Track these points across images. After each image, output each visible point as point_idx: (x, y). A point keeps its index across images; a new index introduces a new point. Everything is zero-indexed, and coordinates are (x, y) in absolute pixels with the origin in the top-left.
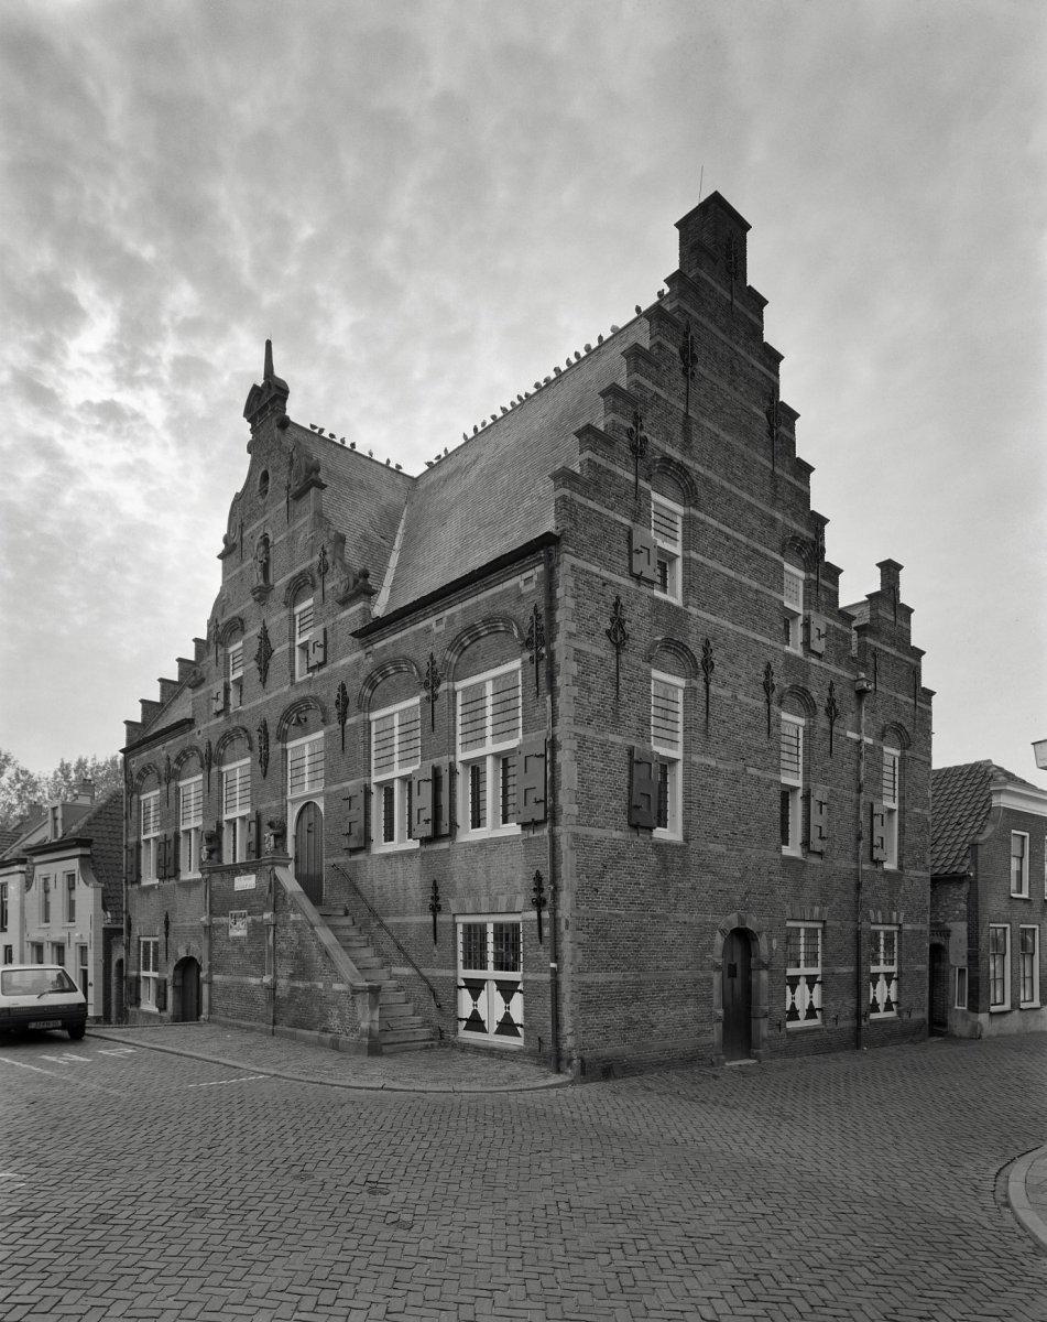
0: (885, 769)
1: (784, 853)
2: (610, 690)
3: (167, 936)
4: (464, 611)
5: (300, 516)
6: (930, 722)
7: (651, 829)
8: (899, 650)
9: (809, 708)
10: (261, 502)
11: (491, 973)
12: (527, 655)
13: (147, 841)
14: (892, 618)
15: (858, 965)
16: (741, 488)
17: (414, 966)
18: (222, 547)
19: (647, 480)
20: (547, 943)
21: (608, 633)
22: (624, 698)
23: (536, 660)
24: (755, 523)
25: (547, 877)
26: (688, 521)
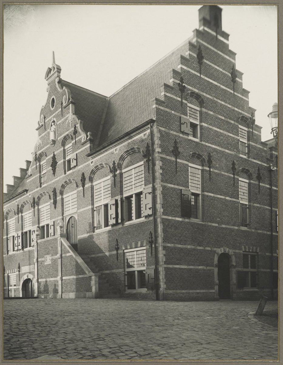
12: (145, 160)
19: (186, 100)
23: (148, 161)
26: (201, 112)
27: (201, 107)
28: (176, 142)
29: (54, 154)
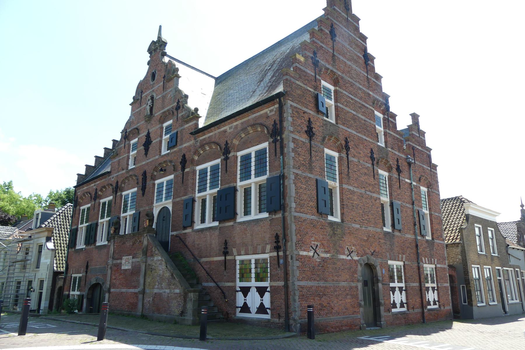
0: (422, 196)
1: (384, 230)
2: (308, 155)
3: (86, 272)
4: (242, 123)
5: (169, 88)
6: (437, 177)
7: (327, 215)
8: (422, 148)
9: (389, 169)
10: (152, 83)
11: (253, 283)
13: (82, 228)
14: (418, 135)
15: (420, 282)
16: (356, 81)
17: (215, 282)
18: (132, 101)
20: (282, 266)
21: (306, 132)
22: (314, 159)
23: (275, 141)
24: (363, 95)
25: (281, 237)
27: (335, 85)
28: (309, 121)
29: (149, 132)
